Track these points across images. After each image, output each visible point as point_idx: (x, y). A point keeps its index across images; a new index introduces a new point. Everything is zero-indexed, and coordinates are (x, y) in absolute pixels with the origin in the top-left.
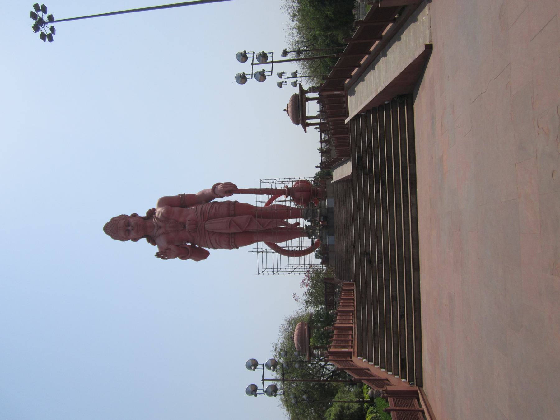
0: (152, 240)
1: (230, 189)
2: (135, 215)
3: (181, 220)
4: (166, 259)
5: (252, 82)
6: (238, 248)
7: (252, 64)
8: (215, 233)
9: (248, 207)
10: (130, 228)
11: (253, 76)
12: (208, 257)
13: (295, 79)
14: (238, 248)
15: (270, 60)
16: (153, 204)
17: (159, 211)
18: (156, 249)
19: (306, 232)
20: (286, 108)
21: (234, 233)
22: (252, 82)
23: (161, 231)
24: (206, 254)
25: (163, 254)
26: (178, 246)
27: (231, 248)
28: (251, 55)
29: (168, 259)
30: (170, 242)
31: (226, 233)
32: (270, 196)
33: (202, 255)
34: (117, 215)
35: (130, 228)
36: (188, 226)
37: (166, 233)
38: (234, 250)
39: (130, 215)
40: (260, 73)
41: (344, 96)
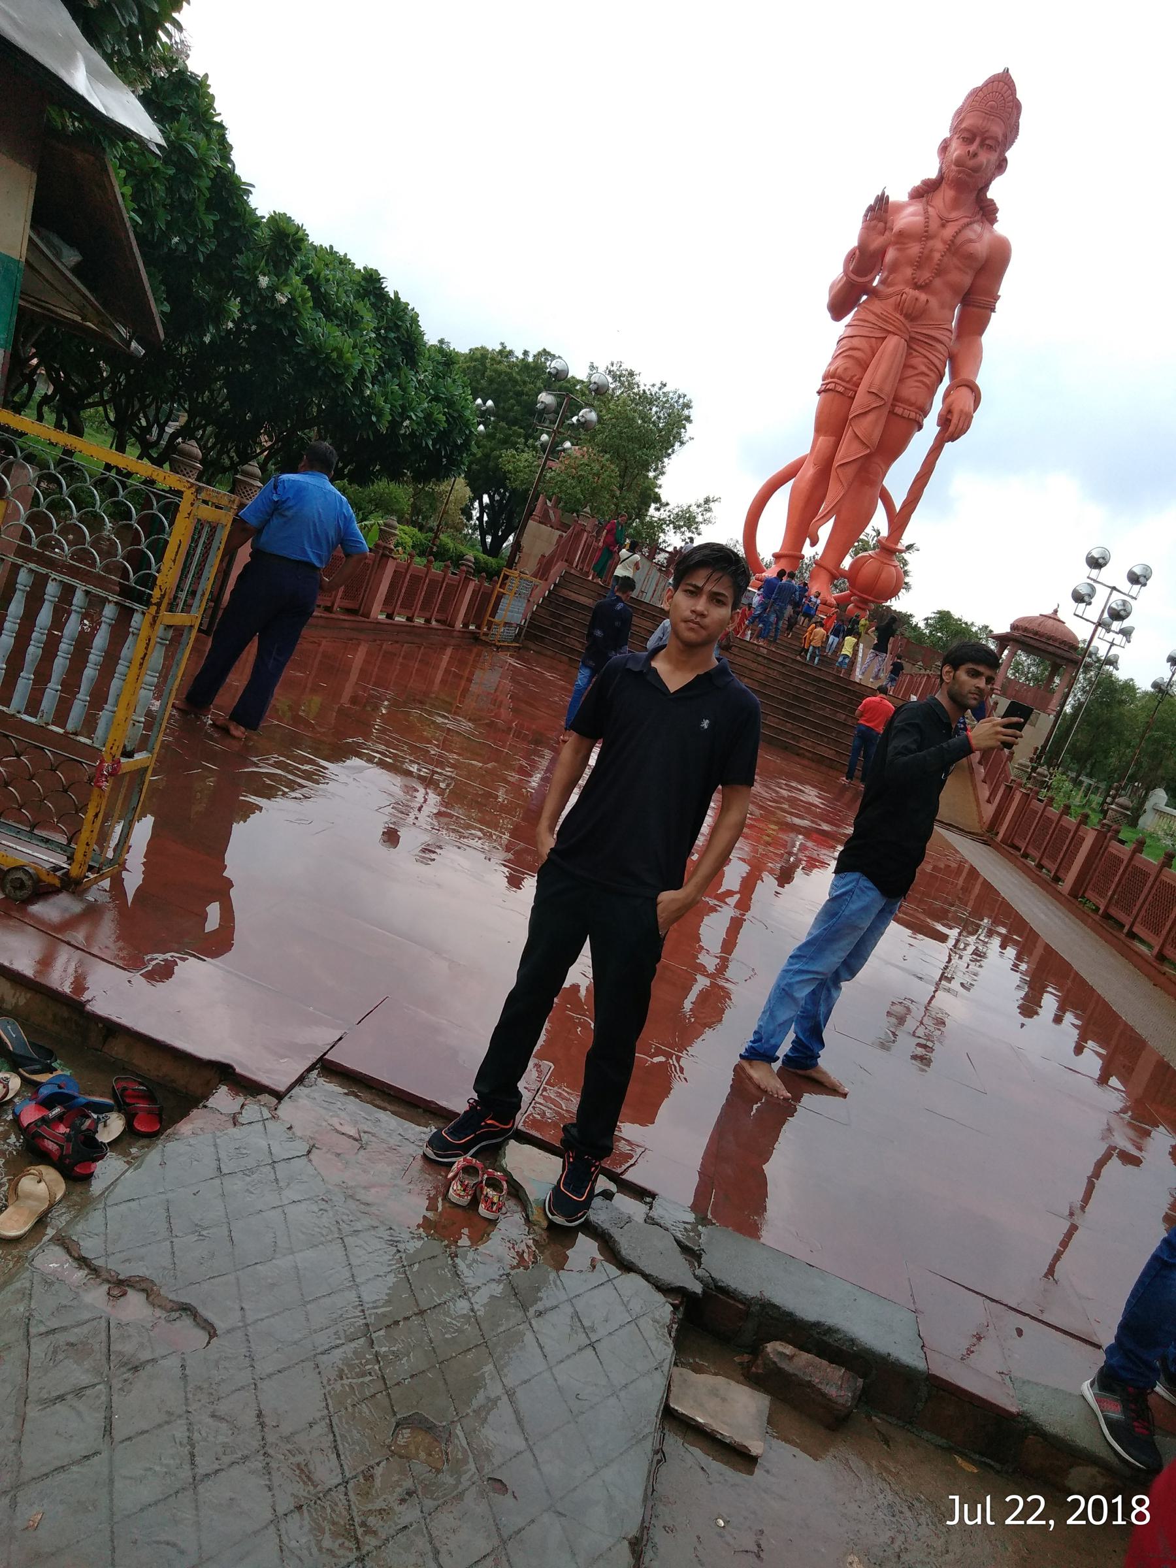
0: (925, 192)
1: (953, 427)
2: (1001, 165)
4: (866, 216)
5: (1081, 575)
6: (819, 393)
7: (1114, 588)
12: (829, 315)
17: (978, 239)
18: (899, 194)
19: (790, 554)
20: (1060, 616)
22: (1081, 575)
25: (880, 210)
28: (1133, 594)
29: (865, 221)
34: (1022, 121)
36: (922, 293)
39: (1008, 154)
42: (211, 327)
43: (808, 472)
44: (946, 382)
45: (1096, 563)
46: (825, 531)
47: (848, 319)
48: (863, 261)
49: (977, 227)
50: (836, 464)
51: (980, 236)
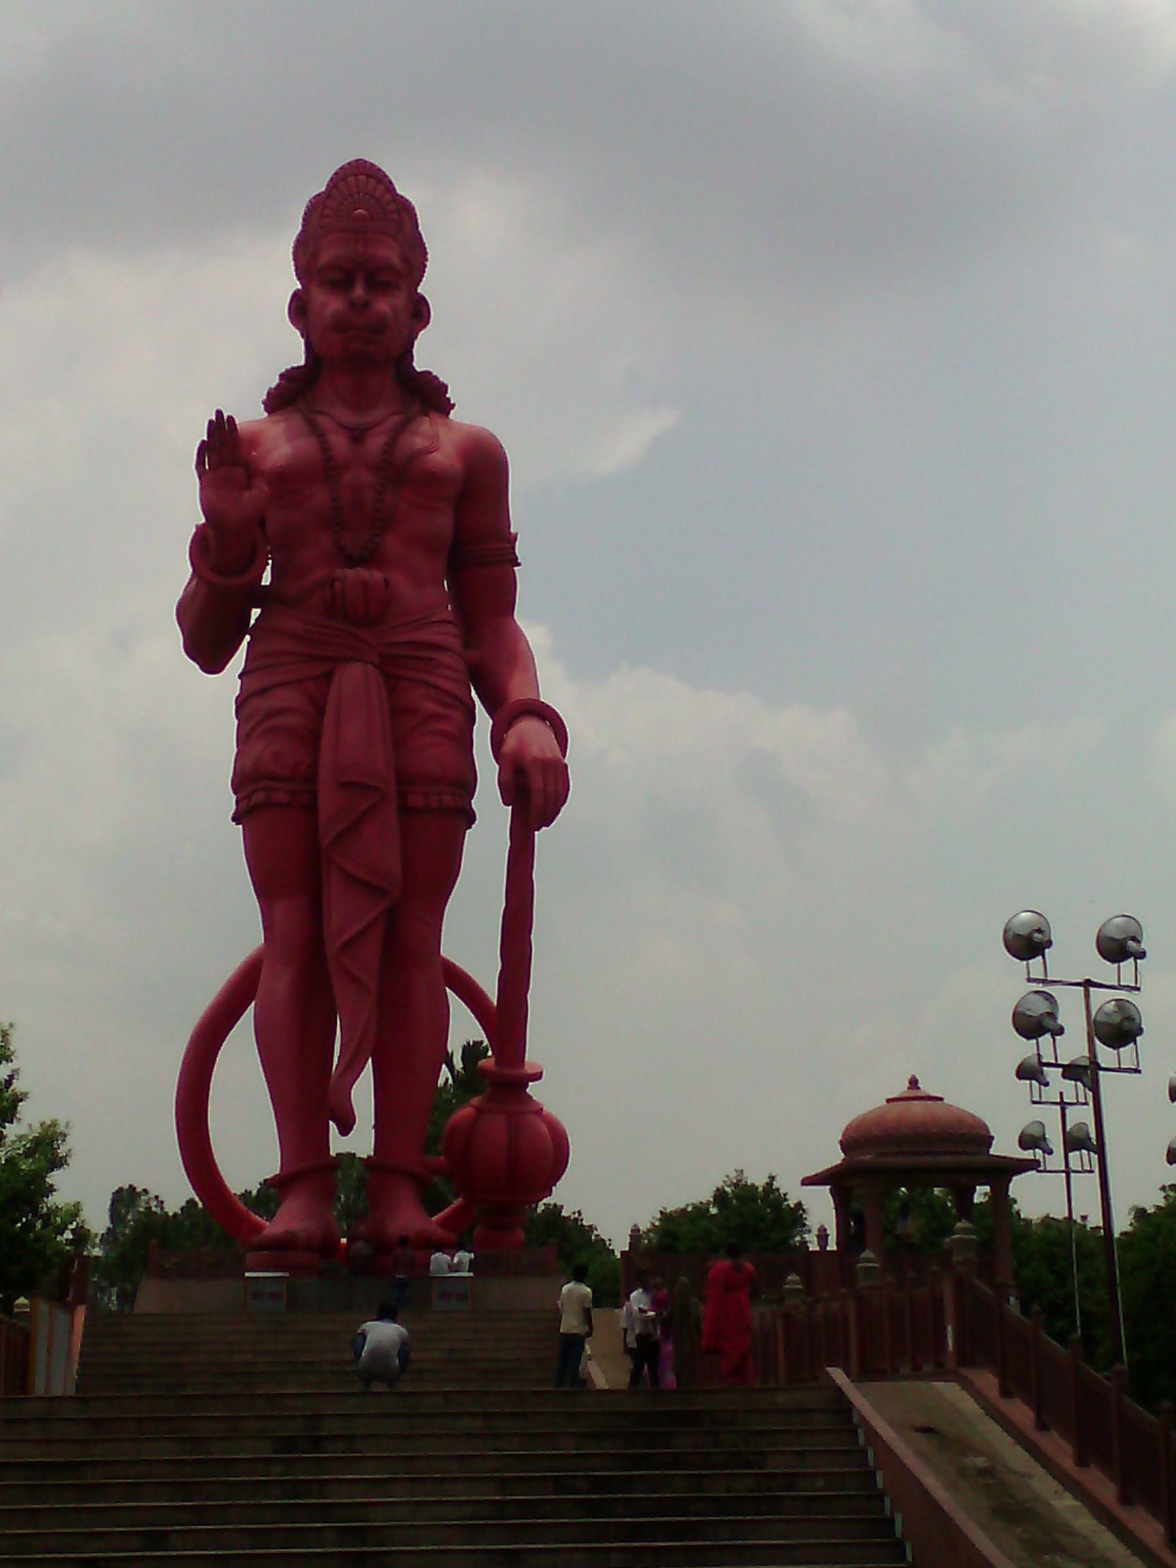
0: (288, 395)
1: (537, 794)
2: (420, 313)
3: (391, 544)
5: (1012, 981)
6: (236, 819)
7: (1088, 984)
8: (319, 708)
9: (438, 873)
10: (359, 291)
11: (1040, 987)
13: (1056, 1141)
14: (236, 819)
15: (1106, 1055)
16: (471, 409)
17: (439, 445)
18: (249, 412)
20: (926, 1087)
21: (312, 808)
22: (1012, 981)
23: (339, 442)
24: (212, 662)
25: (223, 446)
26: (262, 524)
27: (238, 784)
28: (1128, 980)
30: (286, 480)
31: (315, 764)
32: (493, 995)
33: (207, 634)
35: (359, 291)
37: (328, 467)
38: (230, 802)
40: (1052, 1015)
41: (940, 1365)
42: (652, 1313)
43: (277, 983)
44: (483, 723)
45: (1027, 945)
46: (363, 1093)
47: (238, 661)
48: (221, 555)
49: (425, 426)
50: (332, 947)
51: (435, 438)
